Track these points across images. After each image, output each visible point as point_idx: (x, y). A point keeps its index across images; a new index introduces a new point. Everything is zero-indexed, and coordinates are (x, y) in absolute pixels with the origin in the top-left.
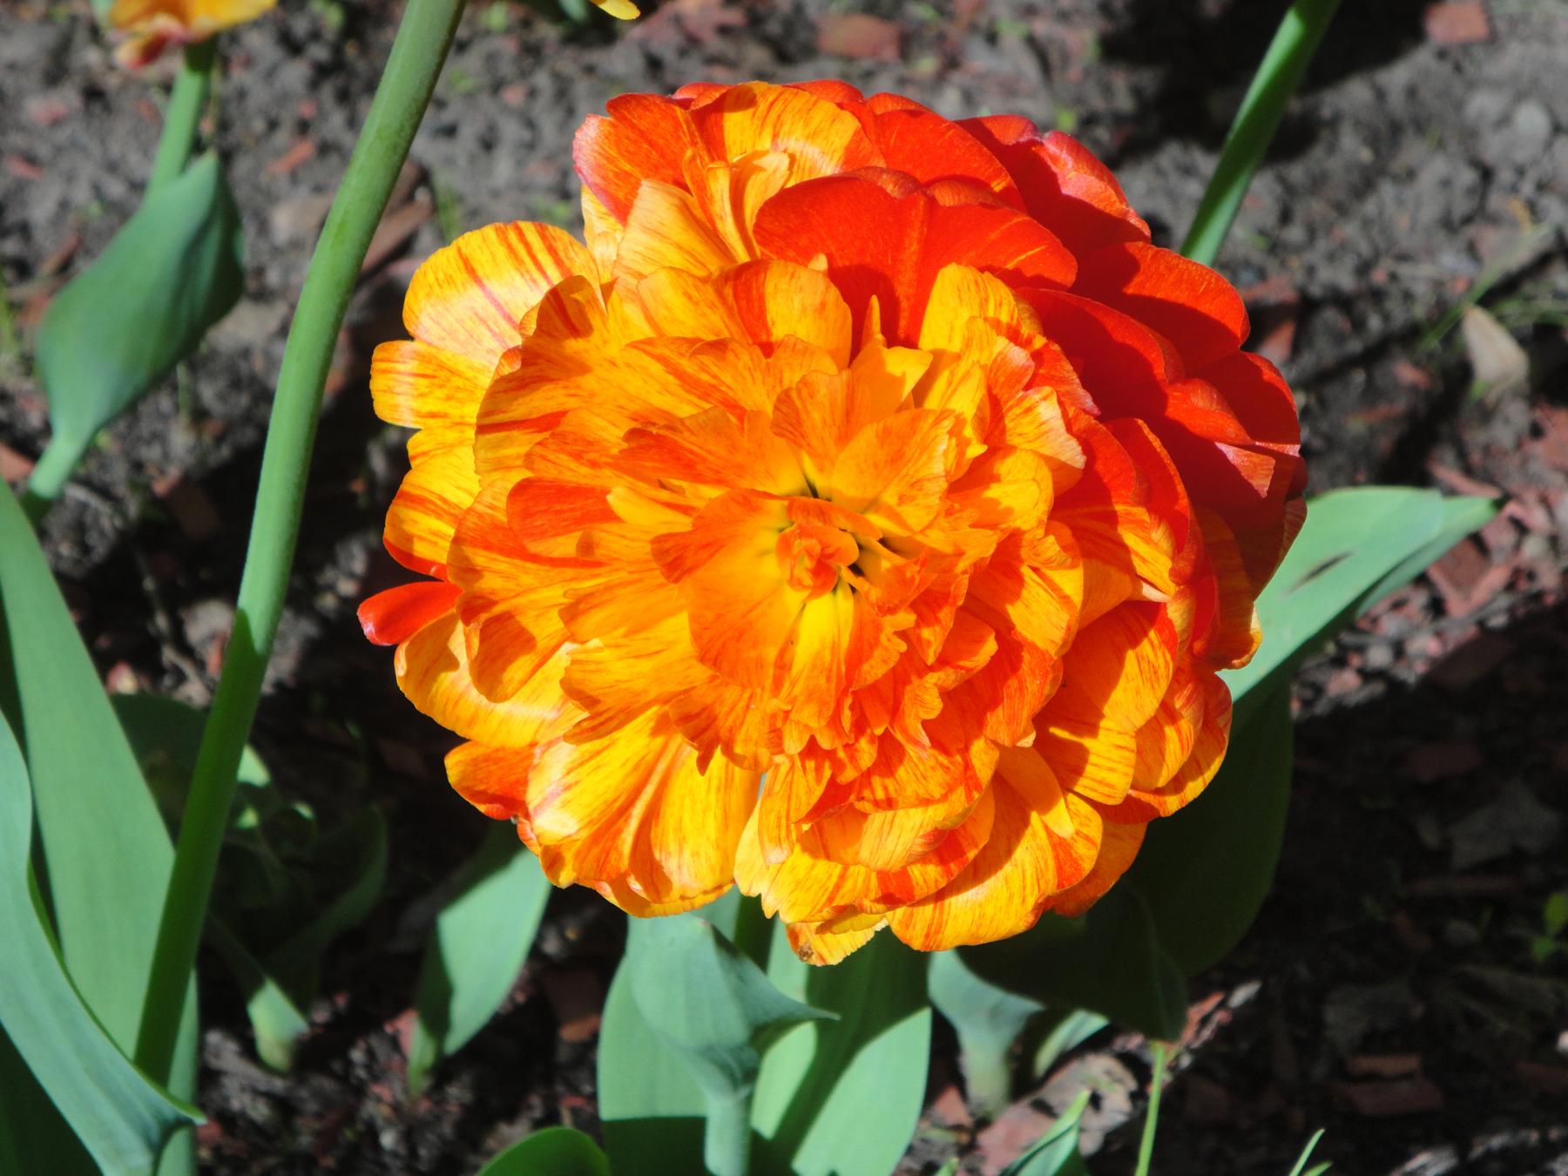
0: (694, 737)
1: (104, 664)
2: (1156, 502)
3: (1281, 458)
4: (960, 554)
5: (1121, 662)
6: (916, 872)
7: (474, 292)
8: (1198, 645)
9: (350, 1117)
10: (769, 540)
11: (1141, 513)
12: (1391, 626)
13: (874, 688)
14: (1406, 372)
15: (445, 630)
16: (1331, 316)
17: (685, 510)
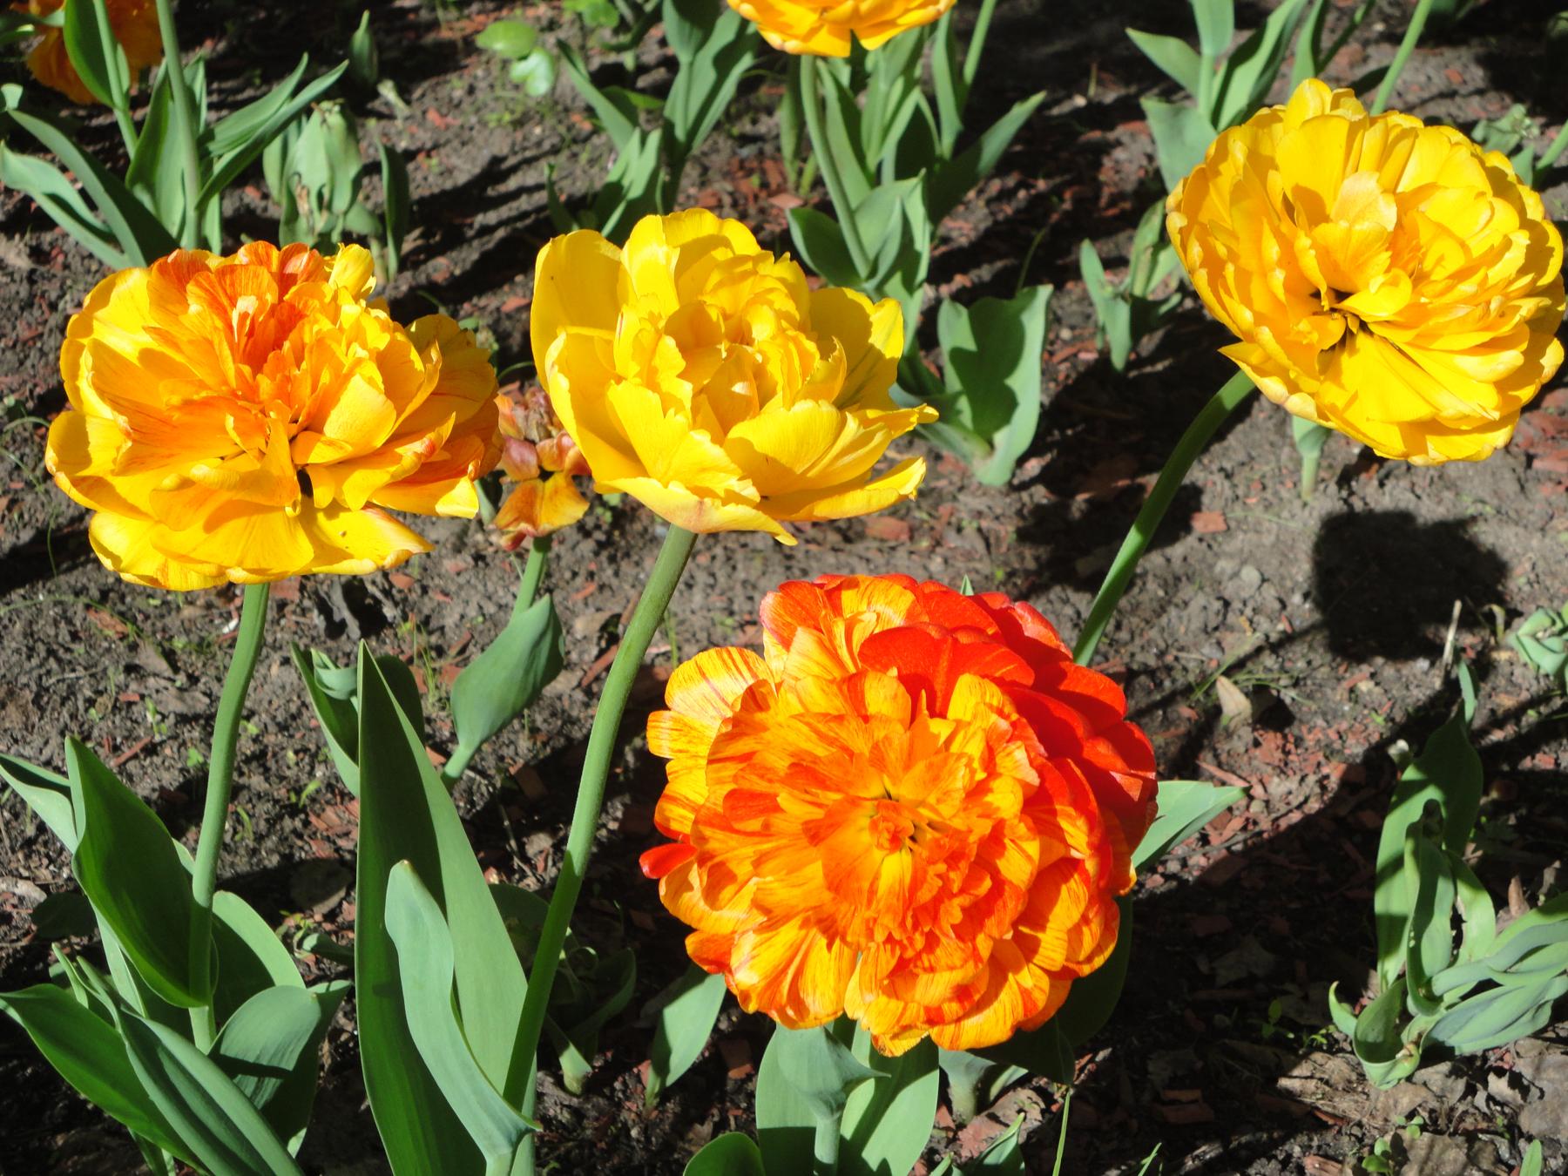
0: (825, 932)
1: (485, 866)
2: (1080, 806)
3: (1145, 779)
4: (970, 831)
5: (1059, 891)
6: (946, 1007)
7: (704, 683)
8: (1102, 884)
9: (613, 1120)
10: (864, 822)
11: (1071, 810)
12: (1179, 851)
13: (924, 907)
14: (1185, 711)
15: (687, 868)
16: (1143, 679)
17: (819, 805)
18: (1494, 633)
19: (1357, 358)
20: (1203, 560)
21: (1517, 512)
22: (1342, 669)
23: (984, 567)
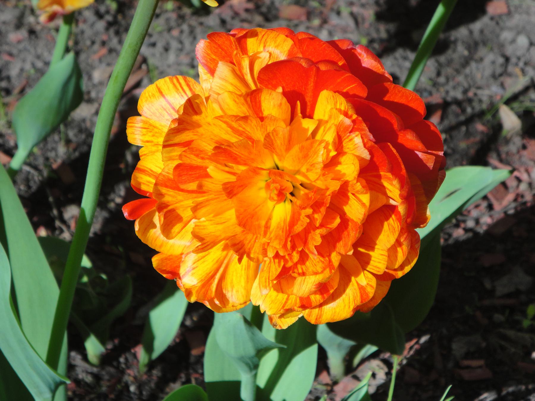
0: (237, 251)
1: (36, 227)
2: (394, 171)
3: (437, 156)
4: (327, 189)
6: (312, 297)
7: (162, 99)
8: (409, 220)
9: (119, 381)
10: (263, 184)
11: (389, 175)
12: (475, 213)
13: (298, 235)
14: (480, 127)
15: (152, 215)
16: (454, 108)
17: (234, 174)
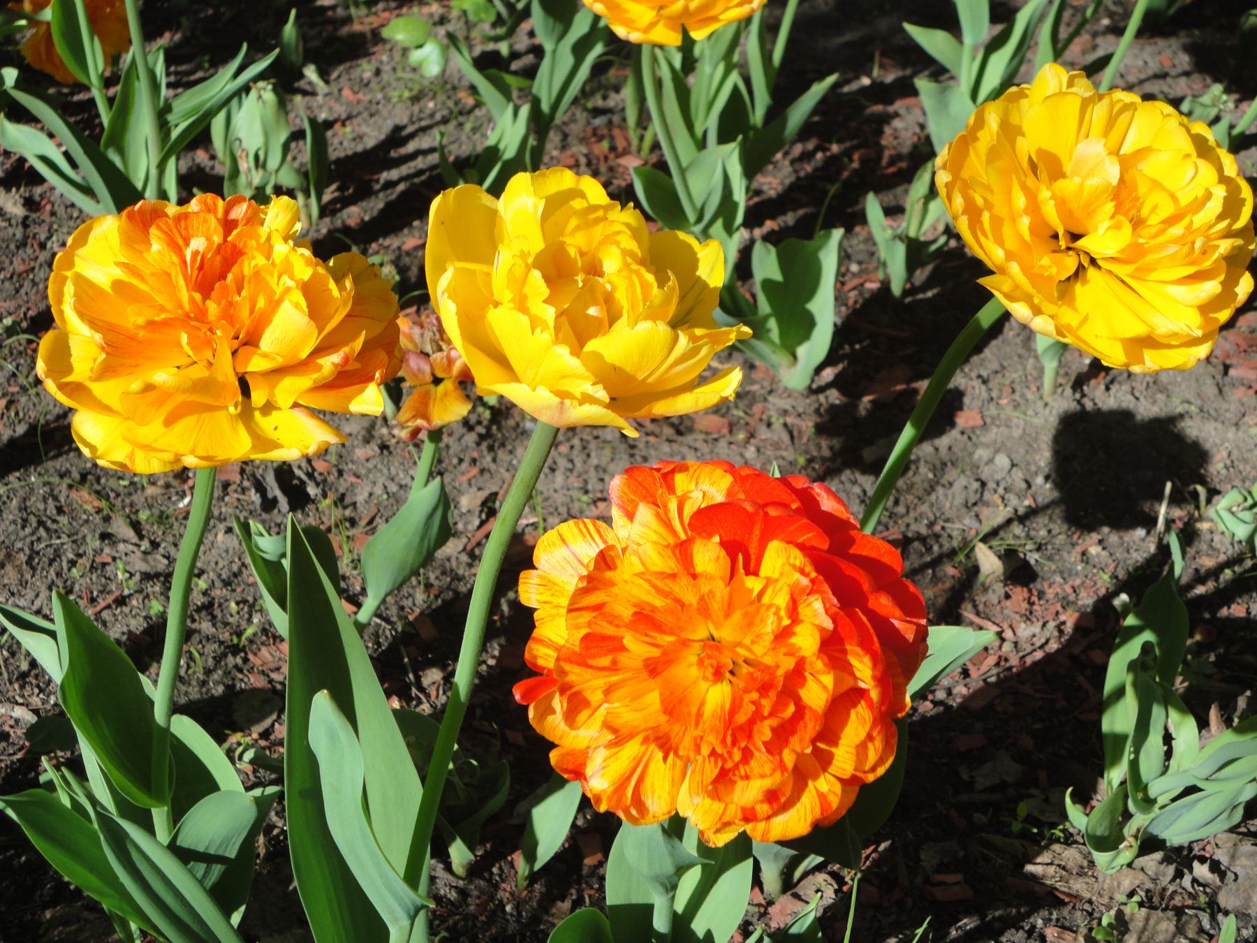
0: (661, 747)
1: (388, 694)
2: (866, 646)
3: (918, 625)
4: (778, 666)
5: (849, 714)
6: (758, 807)
7: (564, 548)
8: (883, 709)
9: (492, 898)
10: (693, 659)
11: (859, 650)
12: (945, 682)
13: (741, 728)
14: (950, 570)
15: (551, 696)
16: (917, 545)
17: (657, 646)
18: (1198, 507)
19: (1087, 287)
20: (965, 449)
21: (1216, 410)
22: (1075, 537)
23: (789, 455)
